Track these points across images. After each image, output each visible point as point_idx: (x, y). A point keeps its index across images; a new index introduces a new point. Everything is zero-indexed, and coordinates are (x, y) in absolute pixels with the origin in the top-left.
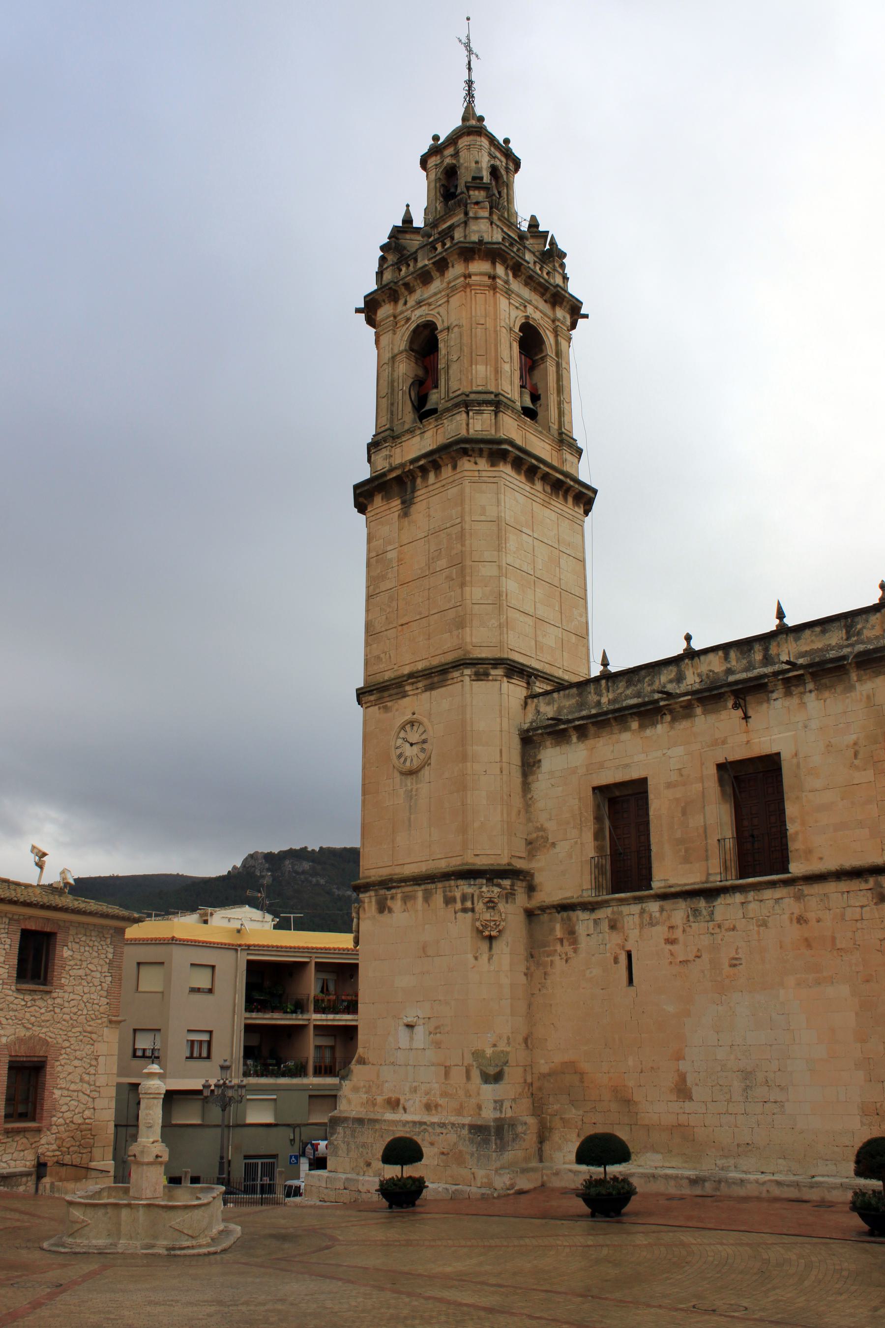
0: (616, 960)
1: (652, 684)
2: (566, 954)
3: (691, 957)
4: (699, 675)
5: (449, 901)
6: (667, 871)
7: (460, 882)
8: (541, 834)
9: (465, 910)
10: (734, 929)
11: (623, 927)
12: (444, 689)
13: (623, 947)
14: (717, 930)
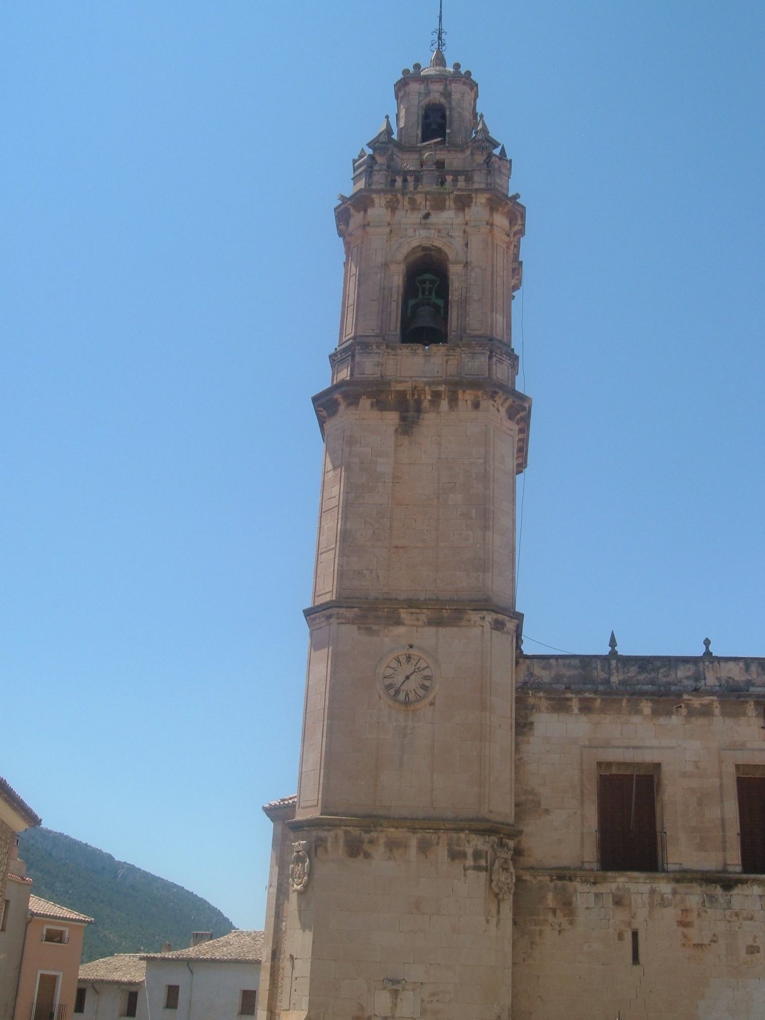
0: (621, 937)
1: (668, 676)
2: (560, 925)
3: (706, 941)
4: (718, 679)
5: (456, 855)
6: (680, 852)
7: (472, 836)
8: (531, 797)
9: (478, 868)
10: (751, 919)
11: (630, 905)
12: (455, 629)
13: (629, 924)
14: (735, 918)
